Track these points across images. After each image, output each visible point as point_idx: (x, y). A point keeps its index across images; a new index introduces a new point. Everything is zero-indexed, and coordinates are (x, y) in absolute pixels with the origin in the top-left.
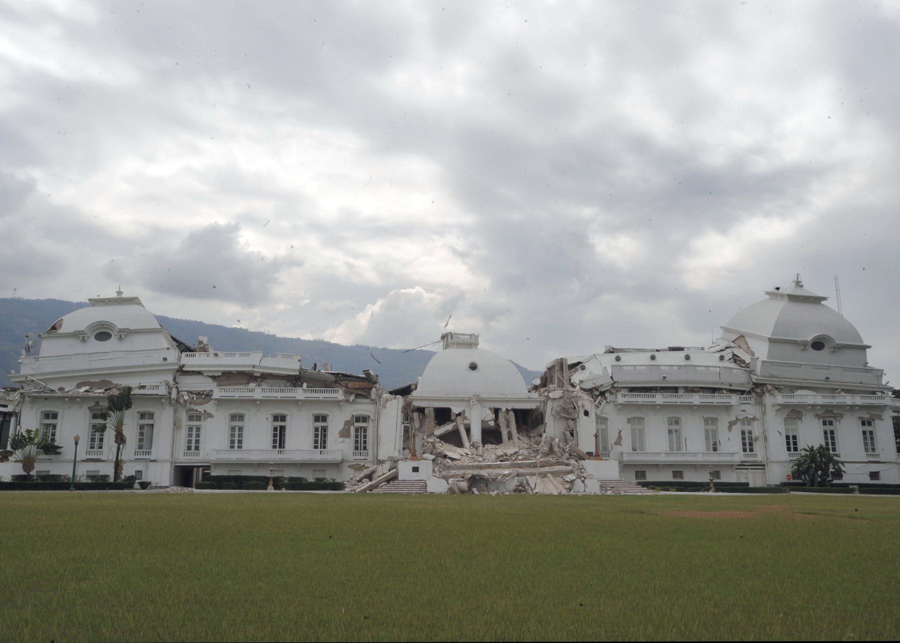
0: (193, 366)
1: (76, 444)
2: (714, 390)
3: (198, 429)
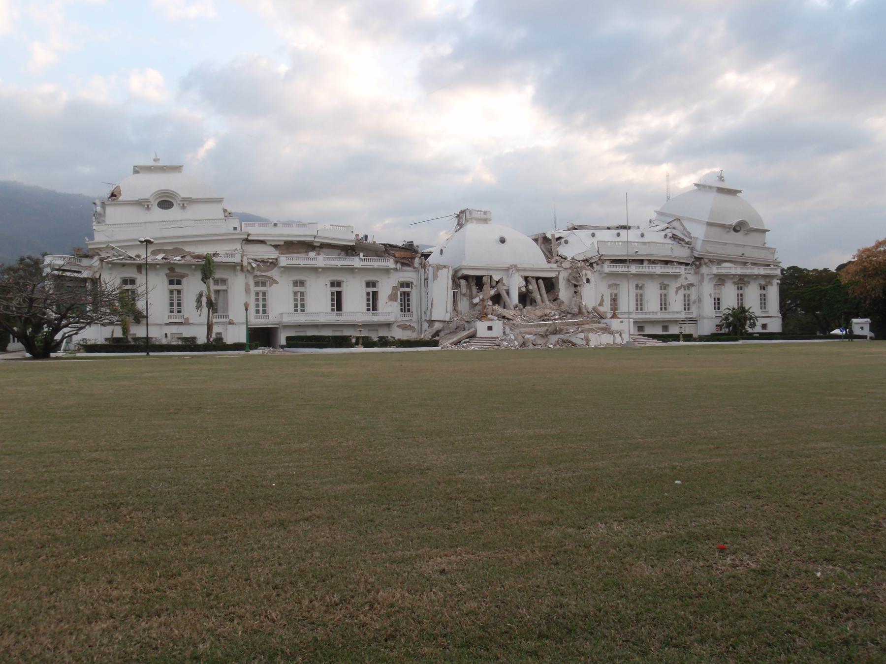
0: (258, 235)
1: (247, 310)
2: (666, 262)
3: (264, 294)
